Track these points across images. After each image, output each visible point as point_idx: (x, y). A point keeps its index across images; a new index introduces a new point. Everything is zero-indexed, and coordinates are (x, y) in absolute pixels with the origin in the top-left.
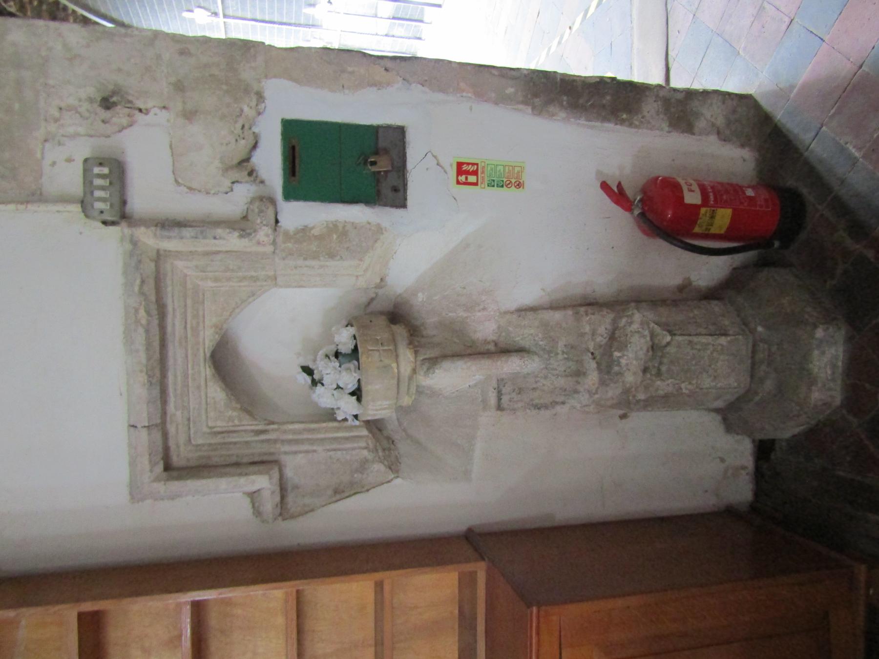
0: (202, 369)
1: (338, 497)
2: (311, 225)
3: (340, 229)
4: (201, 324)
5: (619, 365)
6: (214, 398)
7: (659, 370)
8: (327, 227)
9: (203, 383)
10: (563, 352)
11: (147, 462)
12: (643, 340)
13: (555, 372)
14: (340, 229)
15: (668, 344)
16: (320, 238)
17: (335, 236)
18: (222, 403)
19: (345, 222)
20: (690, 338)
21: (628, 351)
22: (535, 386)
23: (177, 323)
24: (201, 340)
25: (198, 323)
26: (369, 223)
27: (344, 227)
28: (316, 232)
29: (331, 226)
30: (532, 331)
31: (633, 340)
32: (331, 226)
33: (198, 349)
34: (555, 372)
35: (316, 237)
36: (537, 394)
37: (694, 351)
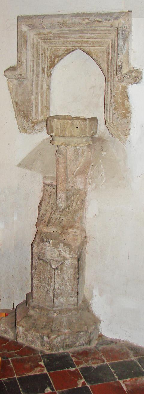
0: (71, 45)
1: (15, 104)
2: (129, 100)
3: (127, 115)
4: (90, 45)
5: (47, 241)
6: (60, 50)
7: (41, 259)
8: (129, 108)
11: (29, 23)
12: (56, 255)
13: (53, 213)
14: (127, 115)
15: (51, 266)
16: (123, 104)
17: (124, 112)
18: (58, 54)
19: (131, 117)
20: (53, 278)
21: (52, 247)
22: (50, 203)
23: (88, 35)
24: (84, 45)
25: (90, 44)
26: (130, 130)
27: (128, 117)
28: (126, 102)
29: (129, 110)
30: (74, 206)
31: (56, 251)
32: (129, 110)
33: (79, 44)
34: (53, 213)
35: (123, 103)
36: (47, 203)
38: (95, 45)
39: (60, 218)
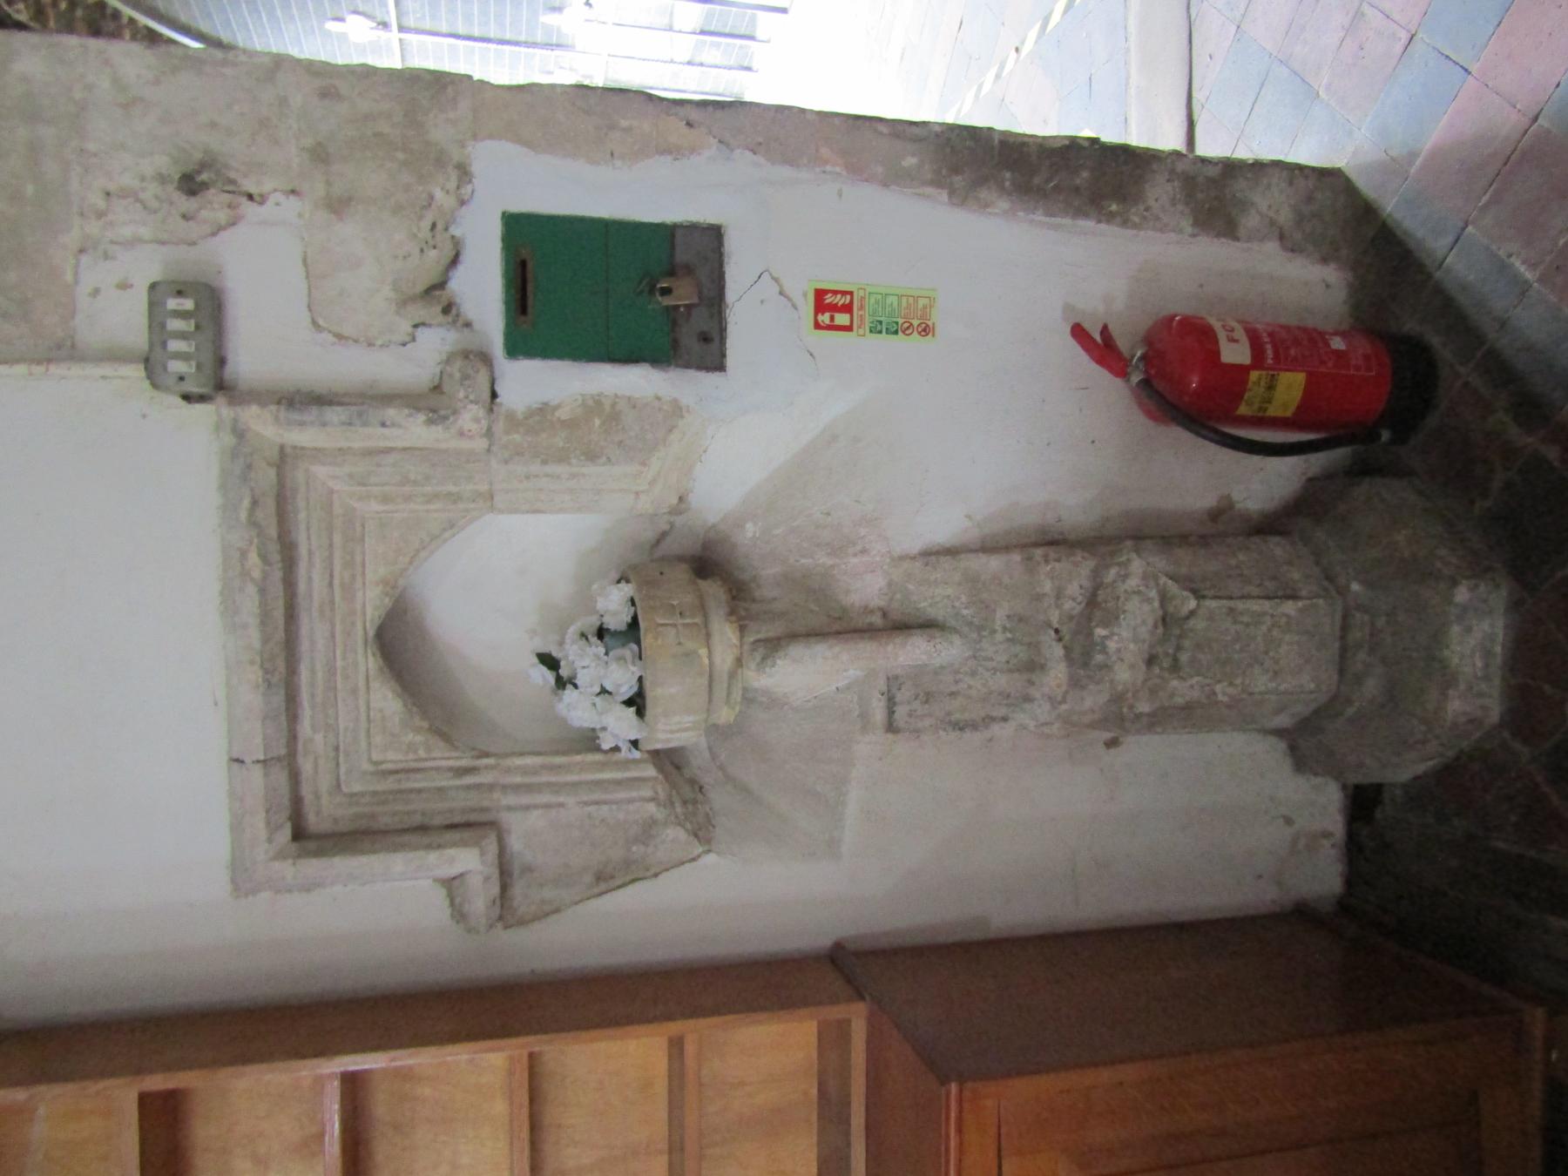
0: (361, 658)
1: (603, 886)
2: (556, 402)
3: (607, 408)
4: (359, 579)
6: (381, 711)
7: (1176, 660)
8: (584, 404)
11: (262, 825)
12: (1146, 608)
13: (990, 664)
14: (607, 408)
15: (1192, 613)
16: (570, 425)
17: (597, 422)
18: (397, 720)
19: (616, 396)
20: (1231, 603)
21: (1120, 626)
22: (954, 689)
23: (316, 577)
24: (359, 607)
25: (353, 577)
26: (658, 399)
27: (614, 405)
28: (563, 414)
29: (590, 402)
30: (949, 591)
32: (590, 402)
33: (353, 624)
34: (990, 664)
35: (564, 424)
36: (957, 703)
38: (358, 559)
39: (1005, 629)
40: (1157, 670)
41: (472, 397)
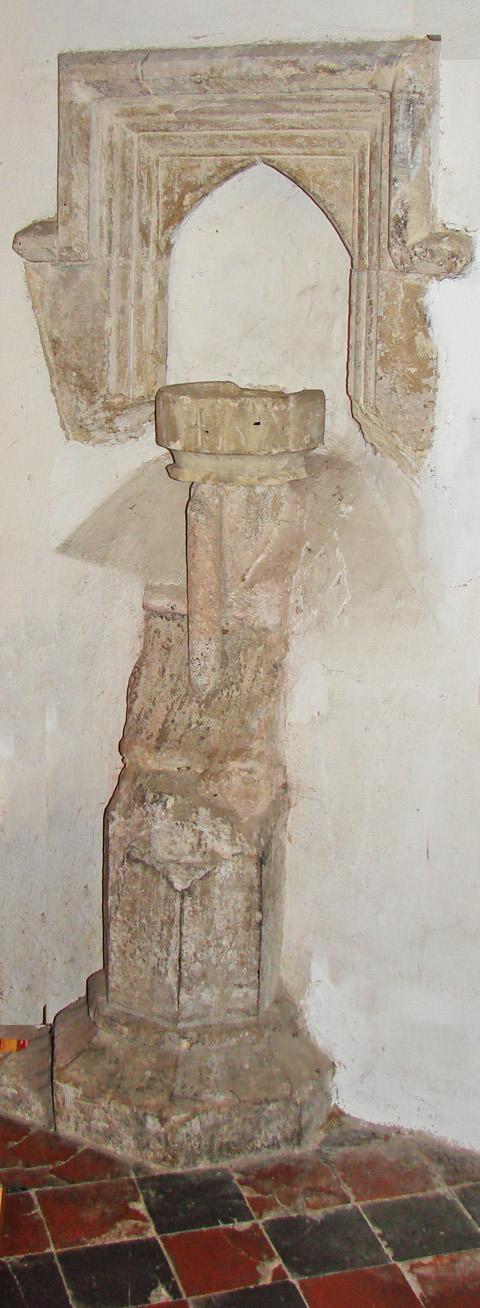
0: (238, 150)
1: (48, 345)
2: (430, 333)
3: (425, 381)
4: (301, 151)
6: (199, 166)
7: (137, 861)
8: (429, 359)
9: (220, 150)
10: (199, 724)
11: (96, 78)
12: (187, 848)
13: (176, 707)
14: (425, 381)
15: (171, 884)
16: (411, 346)
17: (413, 370)
18: (192, 179)
19: (436, 390)
20: (177, 923)
21: (174, 819)
22: (167, 672)
23: (294, 116)
24: (279, 149)
25: (300, 146)
26: (432, 430)
27: (428, 387)
28: (419, 339)
29: (430, 366)
30: (246, 683)
32: (430, 366)
33: (264, 145)
34: (176, 707)
35: (411, 341)
36: (155, 674)
37: (159, 924)
38: (316, 150)
40: (245, 970)
41: (415, 258)
